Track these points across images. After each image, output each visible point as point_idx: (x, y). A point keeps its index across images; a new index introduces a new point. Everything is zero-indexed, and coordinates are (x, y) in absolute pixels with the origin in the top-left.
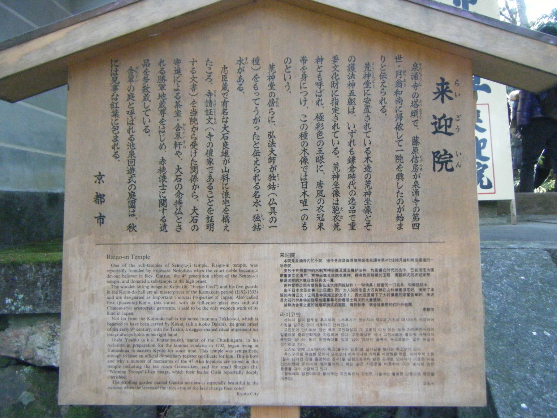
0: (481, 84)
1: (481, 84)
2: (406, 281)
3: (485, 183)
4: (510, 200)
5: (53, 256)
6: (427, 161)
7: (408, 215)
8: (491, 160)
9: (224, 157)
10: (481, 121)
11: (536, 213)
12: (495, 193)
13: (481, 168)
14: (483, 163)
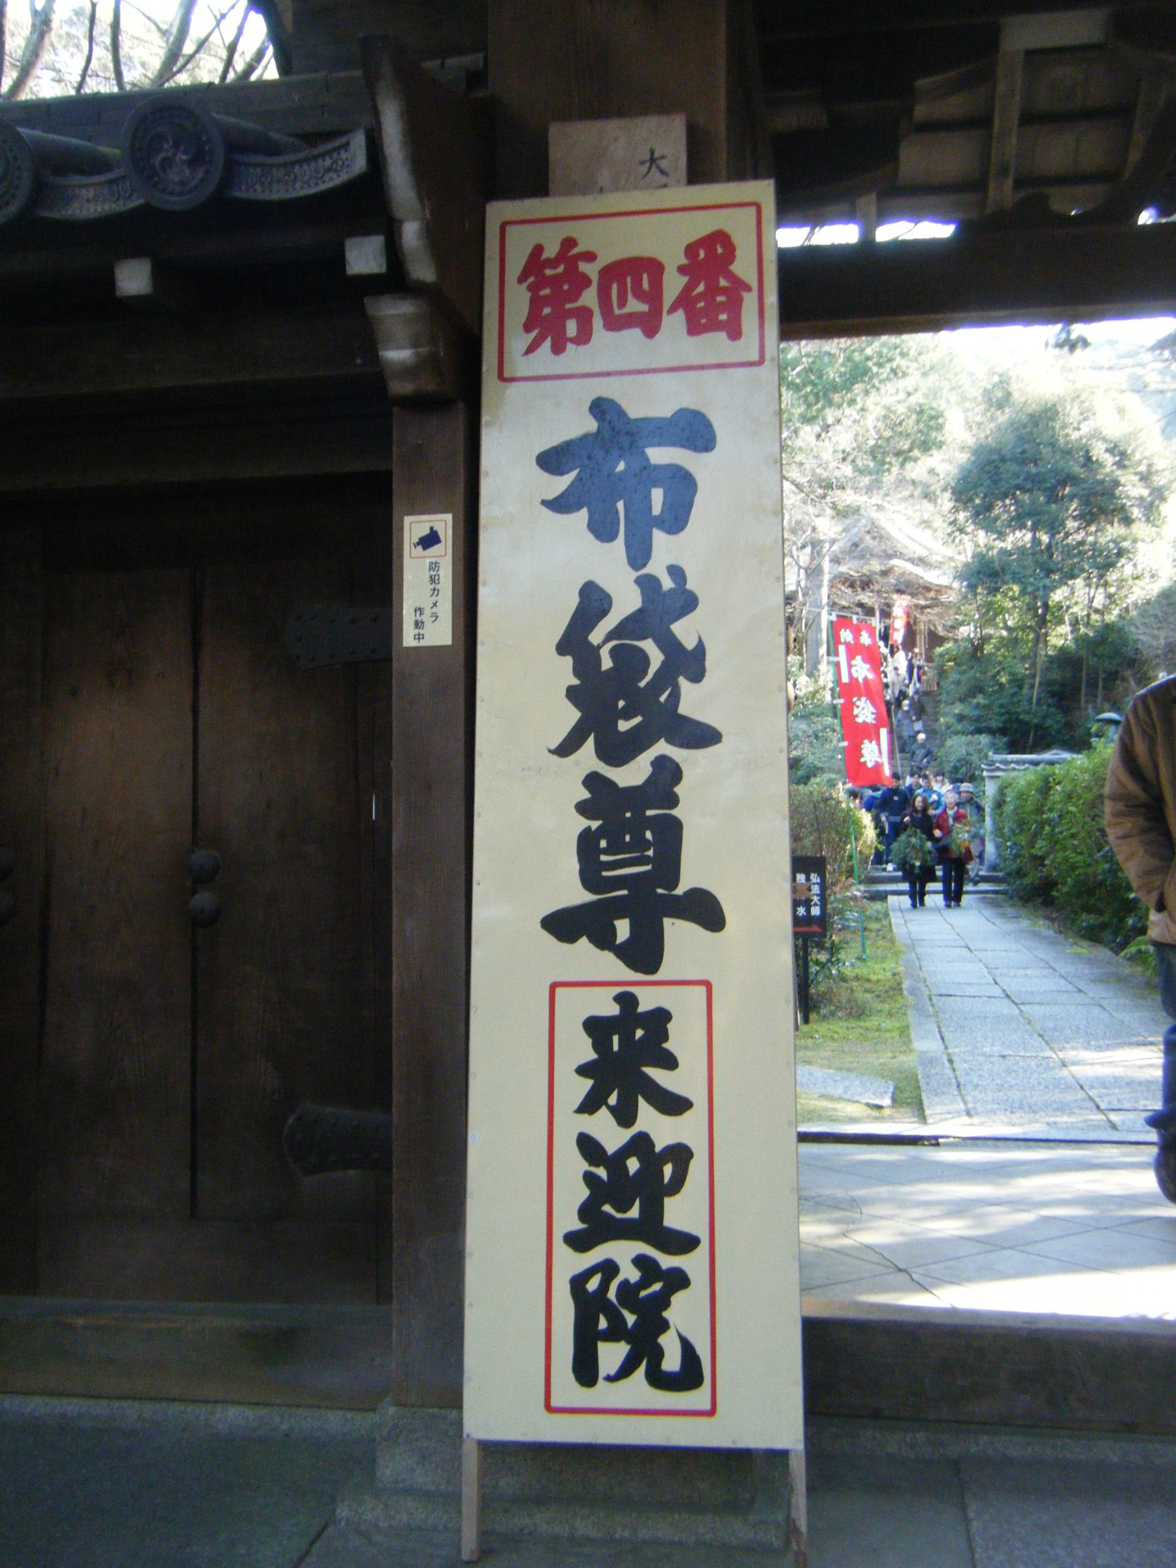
0: (680, 891)
1: (680, 891)
3: (672, 1362)
4: (783, 1454)
5: (722, 159)
8: (703, 1248)
9: (587, 757)
10: (669, 1062)
11: (1004, 1423)
12: (712, 1412)
13: (657, 1287)
14: (667, 1261)
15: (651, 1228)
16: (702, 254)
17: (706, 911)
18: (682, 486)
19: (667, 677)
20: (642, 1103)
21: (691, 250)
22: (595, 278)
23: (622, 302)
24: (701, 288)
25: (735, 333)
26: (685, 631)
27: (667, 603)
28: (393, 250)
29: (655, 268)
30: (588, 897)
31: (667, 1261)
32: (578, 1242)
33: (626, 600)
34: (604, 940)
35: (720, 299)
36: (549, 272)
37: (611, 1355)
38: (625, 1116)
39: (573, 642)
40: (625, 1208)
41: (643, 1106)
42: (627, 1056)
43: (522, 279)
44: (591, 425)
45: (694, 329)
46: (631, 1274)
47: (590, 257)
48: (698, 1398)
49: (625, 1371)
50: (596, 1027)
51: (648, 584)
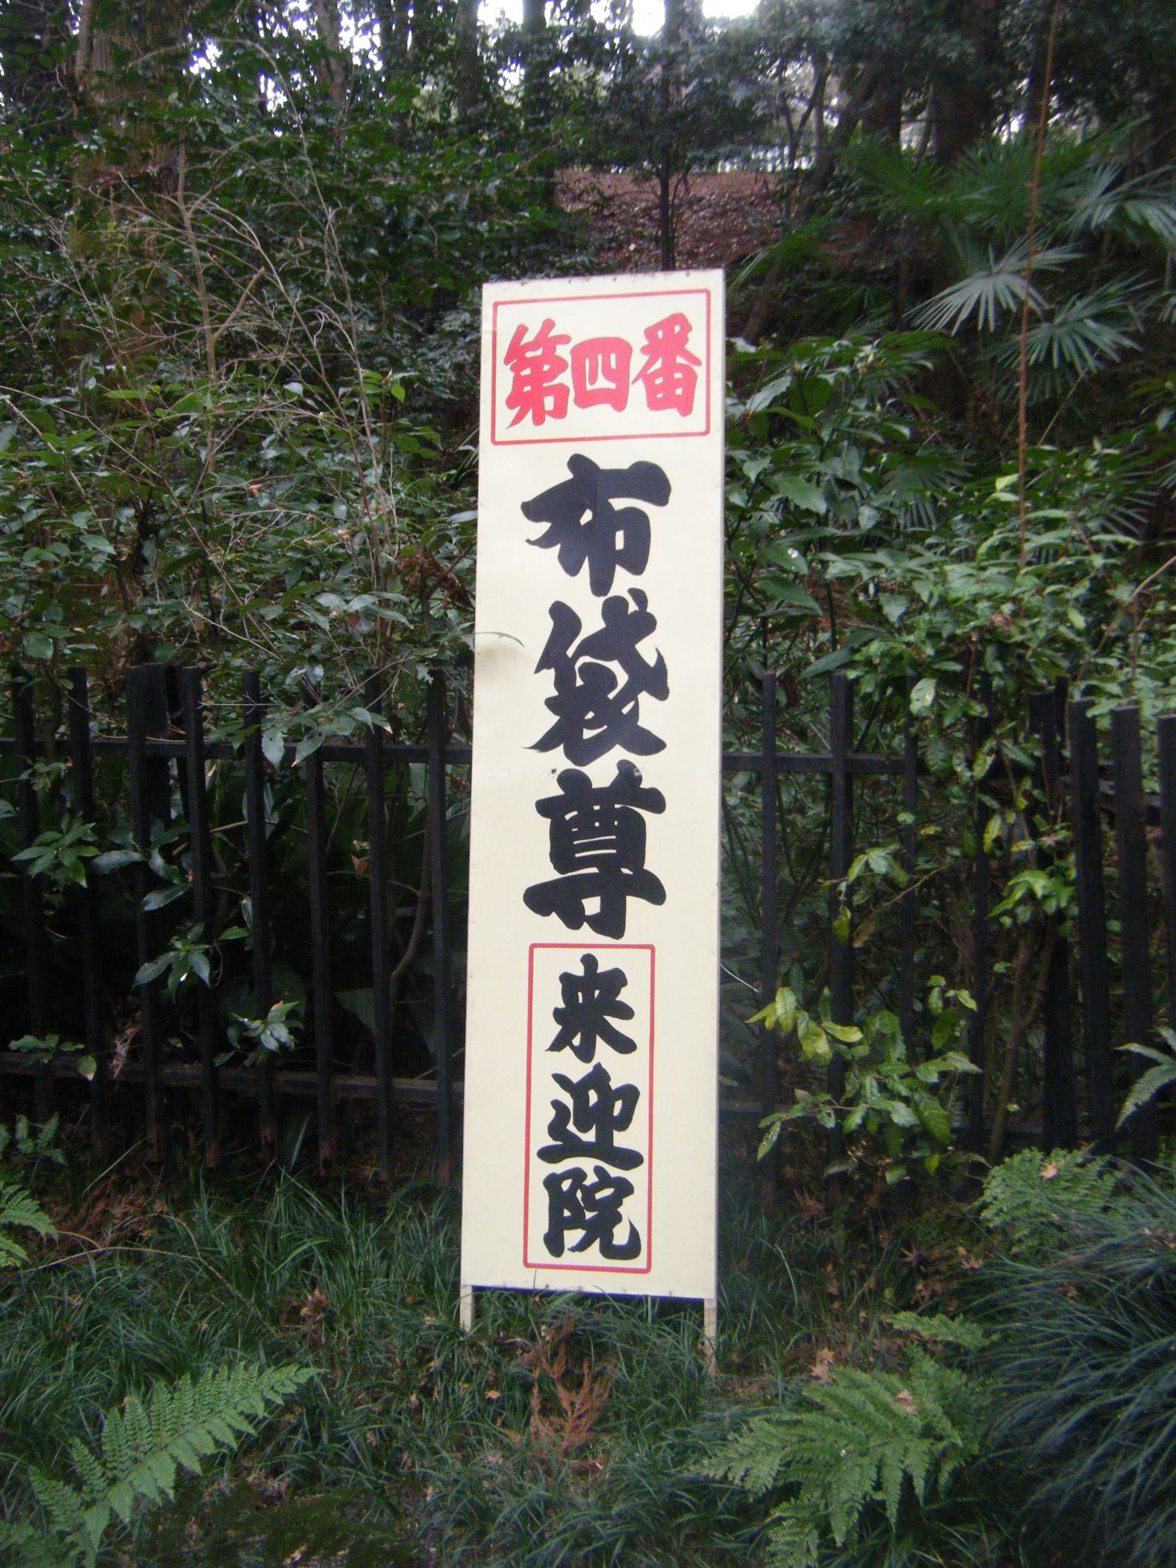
3: (620, 1236)
4: (698, 1305)
8: (644, 1166)
14: (614, 1172)
15: (604, 1150)
16: (660, 334)
17: (654, 891)
18: (638, 527)
19: (630, 693)
20: (599, 1040)
21: (650, 333)
22: (568, 358)
23: (593, 380)
24: (658, 365)
25: (685, 407)
26: (647, 649)
27: (629, 624)
29: (622, 348)
30: (556, 875)
31: (614, 1172)
32: (548, 1155)
33: (592, 622)
34: (574, 918)
35: (678, 375)
36: (529, 354)
37: (573, 1237)
38: (585, 1053)
39: (552, 657)
40: (584, 1129)
41: (600, 1043)
42: (590, 1008)
43: (507, 361)
44: (569, 476)
45: (654, 404)
46: (591, 1179)
47: (565, 339)
48: (640, 1262)
49: (582, 1246)
50: (567, 980)
51: (613, 609)
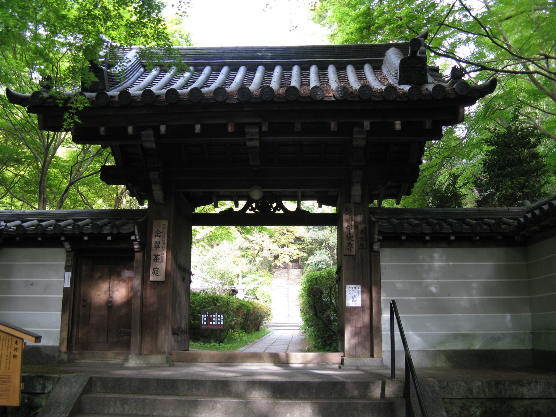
2: (6, 380)
6: (12, 356)
7: (8, 367)
28: (136, 237)
44: (323, 206)
